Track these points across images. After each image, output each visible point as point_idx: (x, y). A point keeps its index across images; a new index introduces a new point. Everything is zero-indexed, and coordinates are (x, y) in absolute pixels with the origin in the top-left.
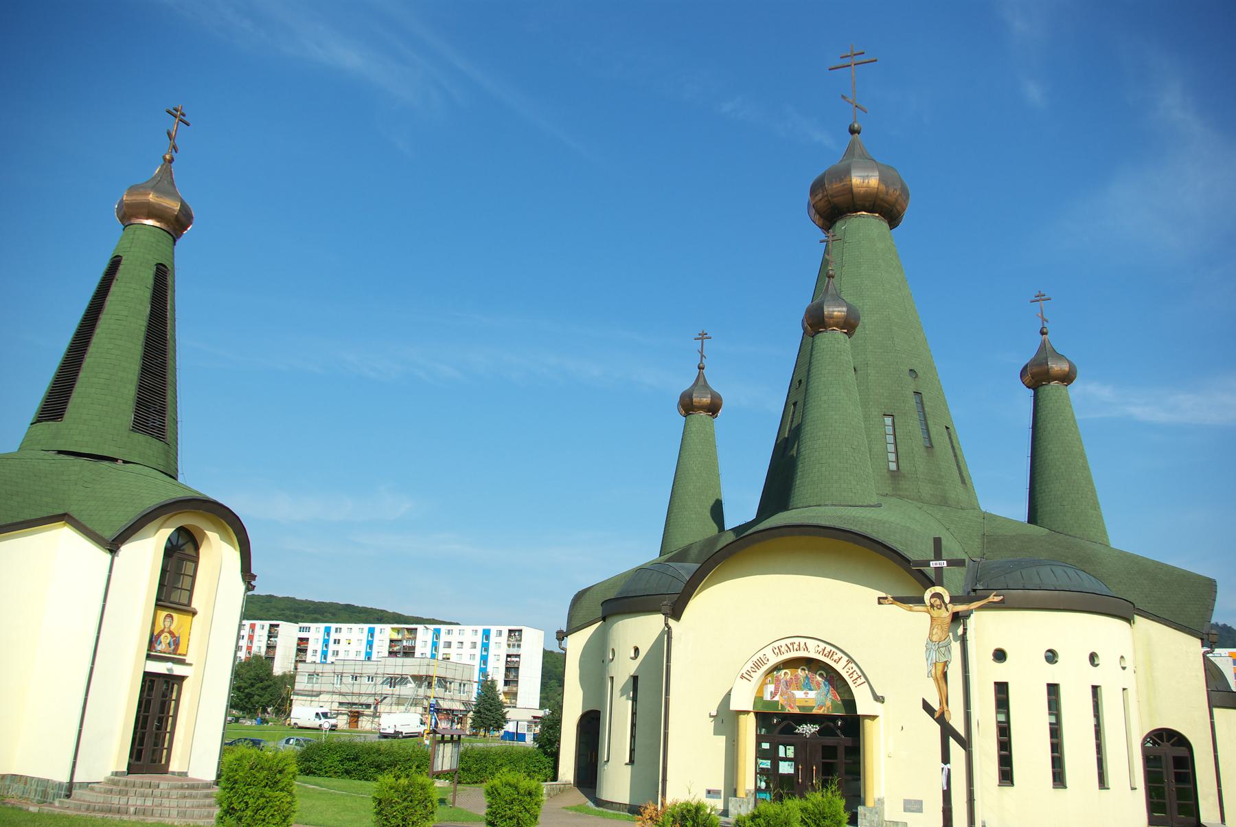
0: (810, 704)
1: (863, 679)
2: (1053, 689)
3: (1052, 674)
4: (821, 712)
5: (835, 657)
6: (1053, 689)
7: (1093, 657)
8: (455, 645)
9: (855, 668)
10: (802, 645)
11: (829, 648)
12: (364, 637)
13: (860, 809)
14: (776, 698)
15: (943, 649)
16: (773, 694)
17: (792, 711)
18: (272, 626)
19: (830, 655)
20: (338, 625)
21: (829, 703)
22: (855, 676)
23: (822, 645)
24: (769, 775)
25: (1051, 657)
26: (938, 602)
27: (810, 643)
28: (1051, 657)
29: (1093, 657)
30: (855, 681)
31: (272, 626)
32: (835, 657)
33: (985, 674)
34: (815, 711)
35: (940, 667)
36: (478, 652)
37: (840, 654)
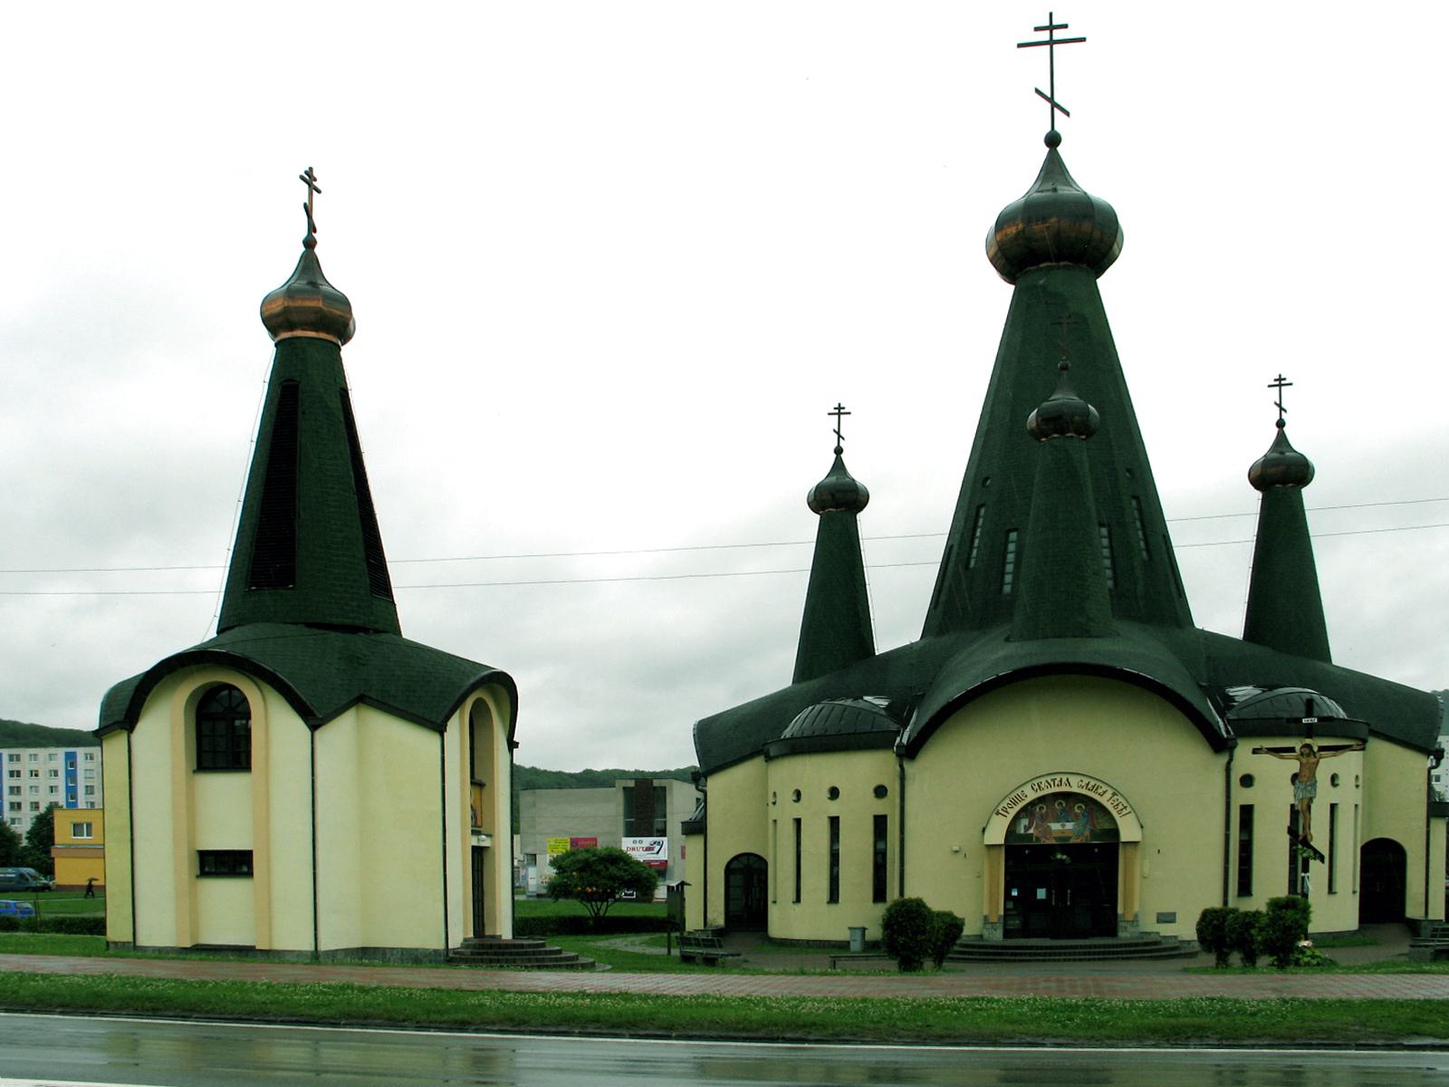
0: (1067, 834)
1: (1129, 809)
2: (834, 822)
3: (834, 808)
4: (1078, 841)
5: (1100, 791)
6: (834, 822)
7: (798, 794)
8: (25, 774)
9: (1121, 799)
10: (1064, 780)
11: (1093, 783)
12: (60, 764)
13: (257, 948)
14: (1031, 831)
15: (1309, 788)
16: (1027, 828)
17: (1048, 842)
18: (67, 754)
19: (1095, 789)
20: (15, 751)
21: (1087, 833)
22: (1120, 807)
23: (1086, 780)
24: (1006, 909)
25: (834, 793)
26: (1307, 751)
27: (1074, 780)
28: (834, 793)
29: (798, 794)
30: (1119, 812)
31: (67, 754)
32: (1100, 791)
33: (786, 811)
34: (1072, 841)
35: (1306, 802)
36: (61, 781)
37: (1105, 788)
